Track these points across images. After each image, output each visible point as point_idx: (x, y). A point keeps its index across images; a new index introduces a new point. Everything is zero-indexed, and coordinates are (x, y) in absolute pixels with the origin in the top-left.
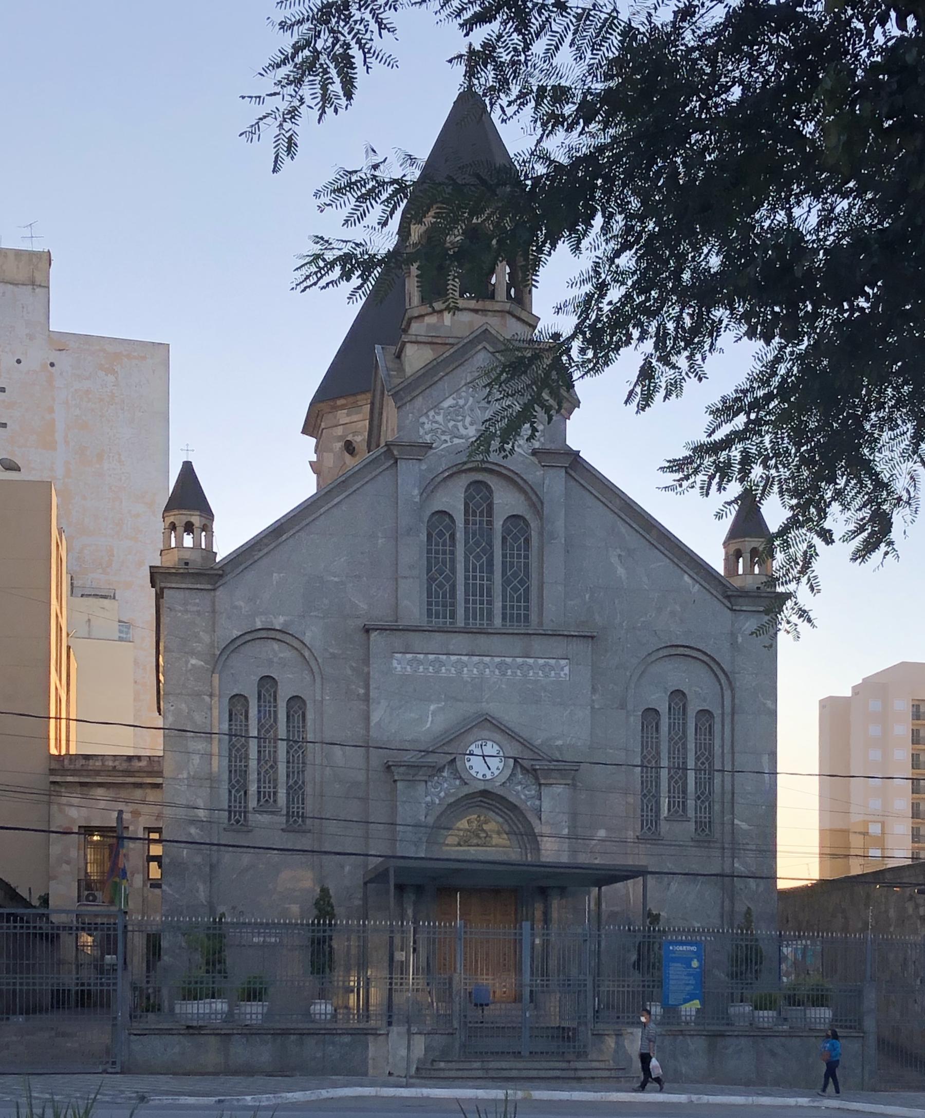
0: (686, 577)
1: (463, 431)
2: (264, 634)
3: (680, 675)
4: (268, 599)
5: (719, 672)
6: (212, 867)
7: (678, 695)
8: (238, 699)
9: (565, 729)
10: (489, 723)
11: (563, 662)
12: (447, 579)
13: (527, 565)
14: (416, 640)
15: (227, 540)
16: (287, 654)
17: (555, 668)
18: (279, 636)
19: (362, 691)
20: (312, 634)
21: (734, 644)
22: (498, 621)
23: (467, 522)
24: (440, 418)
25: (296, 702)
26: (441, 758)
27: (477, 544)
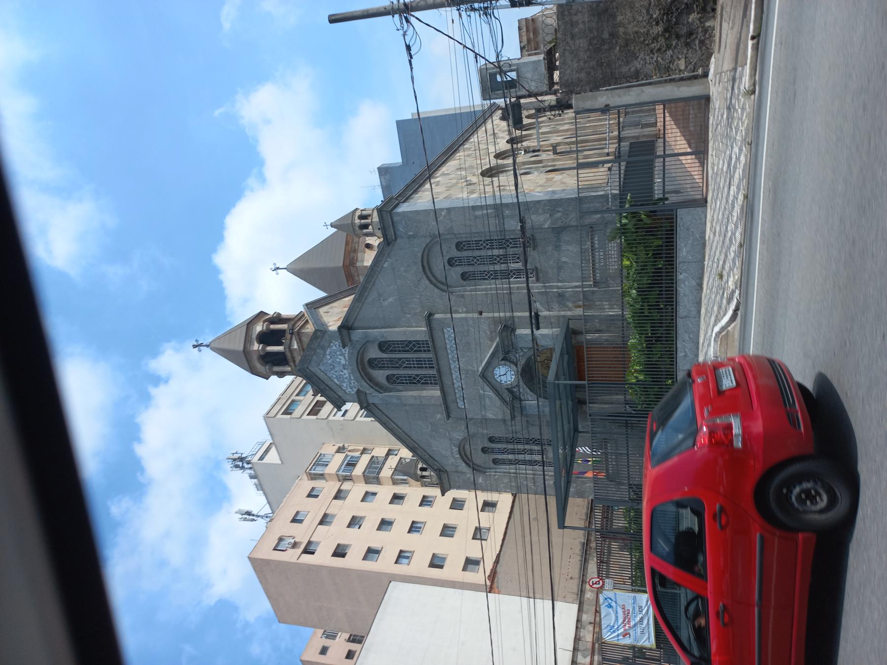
8: (495, 461)
11: (445, 330)
21: (414, 237)
25: (491, 440)
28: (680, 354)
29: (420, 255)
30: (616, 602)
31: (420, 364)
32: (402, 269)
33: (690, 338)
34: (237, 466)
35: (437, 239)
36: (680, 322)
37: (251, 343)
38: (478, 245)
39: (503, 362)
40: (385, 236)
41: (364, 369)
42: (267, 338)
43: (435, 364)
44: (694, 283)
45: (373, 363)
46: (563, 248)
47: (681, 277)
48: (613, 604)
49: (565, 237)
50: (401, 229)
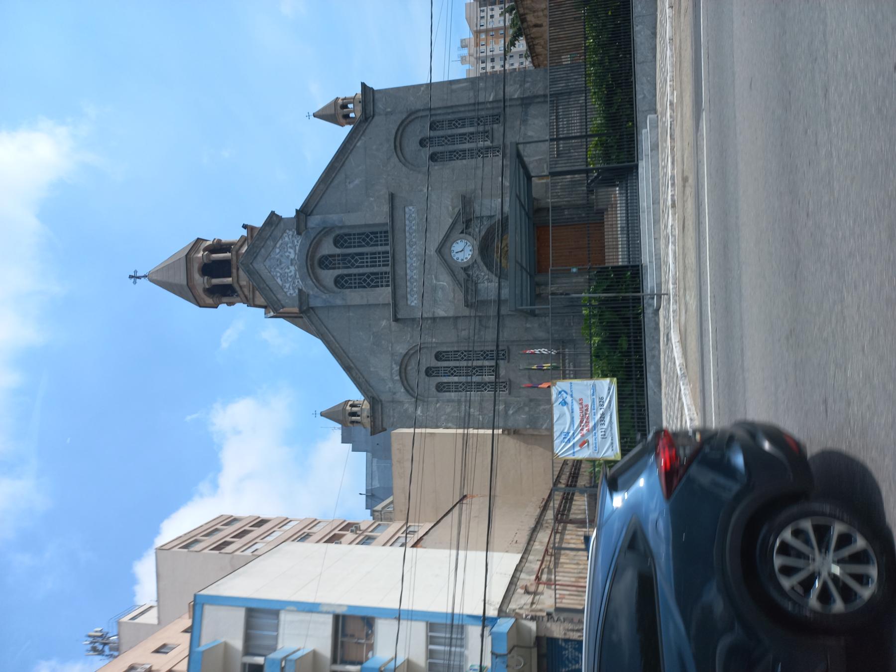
0: (358, 144)
1: (293, 273)
2: (403, 375)
3: (411, 144)
4: (384, 370)
5: (408, 120)
6: (531, 400)
7: (422, 143)
9: (445, 210)
10: (443, 249)
11: (407, 210)
12: (368, 277)
13: (359, 234)
14: (400, 292)
15: (355, 395)
16: (413, 364)
17: (411, 215)
18: (404, 366)
19: (429, 321)
20: (401, 349)
21: (391, 113)
22: (388, 248)
23: (339, 268)
24: (287, 285)
25: (438, 356)
26: (465, 278)
27: (349, 262)
28: (639, 97)
29: (394, 132)
30: (572, 396)
31: (374, 259)
32: (374, 147)
33: (648, 81)
34: (94, 649)
35: (411, 117)
36: (638, 68)
37: (197, 251)
38: (452, 124)
39: (462, 235)
40: (364, 109)
41: (312, 266)
42: (211, 269)
43: (392, 259)
44: (649, 32)
45: (326, 262)
46: (530, 122)
47: (637, 29)
48: (569, 399)
49: (533, 110)
50: (380, 105)
